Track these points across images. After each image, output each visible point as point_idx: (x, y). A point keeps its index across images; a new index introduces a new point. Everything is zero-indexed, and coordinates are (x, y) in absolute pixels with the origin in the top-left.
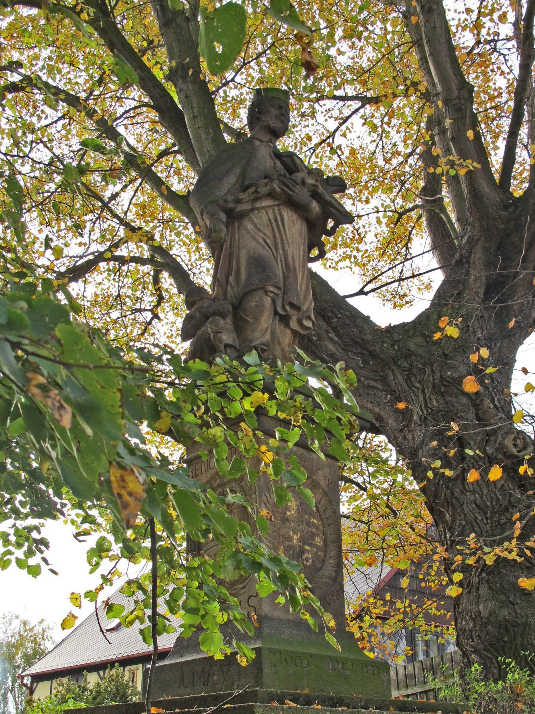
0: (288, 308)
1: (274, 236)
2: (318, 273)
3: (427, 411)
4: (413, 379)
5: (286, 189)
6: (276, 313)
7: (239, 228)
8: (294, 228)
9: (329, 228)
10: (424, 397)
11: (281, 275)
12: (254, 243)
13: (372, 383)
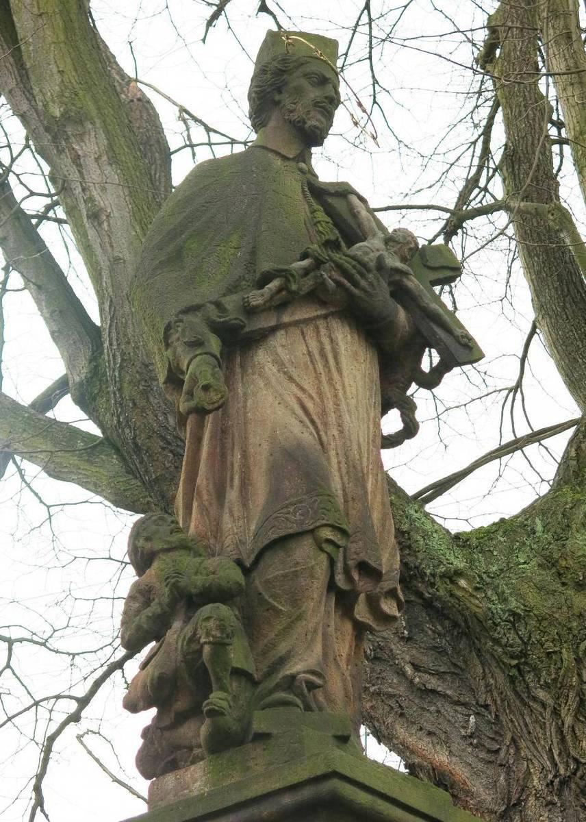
0: (356, 576)
1: (320, 394)
2: (23, 128)
3: (568, 765)
4: (529, 677)
5: (348, 284)
6: (331, 586)
7: (243, 367)
8: (355, 366)
9: (425, 366)
10: (560, 731)
11: (340, 493)
12: (280, 411)
13: (433, 683)
